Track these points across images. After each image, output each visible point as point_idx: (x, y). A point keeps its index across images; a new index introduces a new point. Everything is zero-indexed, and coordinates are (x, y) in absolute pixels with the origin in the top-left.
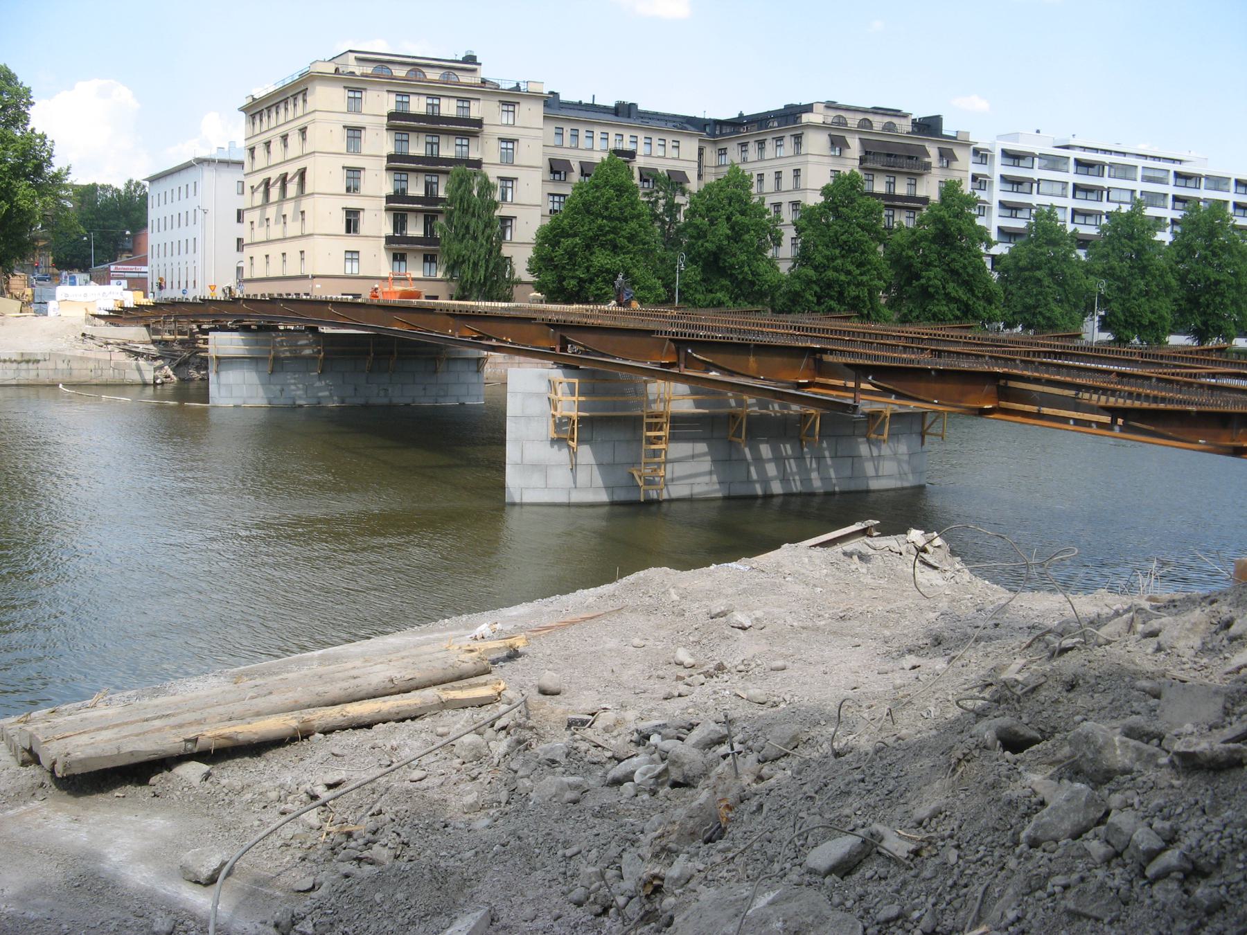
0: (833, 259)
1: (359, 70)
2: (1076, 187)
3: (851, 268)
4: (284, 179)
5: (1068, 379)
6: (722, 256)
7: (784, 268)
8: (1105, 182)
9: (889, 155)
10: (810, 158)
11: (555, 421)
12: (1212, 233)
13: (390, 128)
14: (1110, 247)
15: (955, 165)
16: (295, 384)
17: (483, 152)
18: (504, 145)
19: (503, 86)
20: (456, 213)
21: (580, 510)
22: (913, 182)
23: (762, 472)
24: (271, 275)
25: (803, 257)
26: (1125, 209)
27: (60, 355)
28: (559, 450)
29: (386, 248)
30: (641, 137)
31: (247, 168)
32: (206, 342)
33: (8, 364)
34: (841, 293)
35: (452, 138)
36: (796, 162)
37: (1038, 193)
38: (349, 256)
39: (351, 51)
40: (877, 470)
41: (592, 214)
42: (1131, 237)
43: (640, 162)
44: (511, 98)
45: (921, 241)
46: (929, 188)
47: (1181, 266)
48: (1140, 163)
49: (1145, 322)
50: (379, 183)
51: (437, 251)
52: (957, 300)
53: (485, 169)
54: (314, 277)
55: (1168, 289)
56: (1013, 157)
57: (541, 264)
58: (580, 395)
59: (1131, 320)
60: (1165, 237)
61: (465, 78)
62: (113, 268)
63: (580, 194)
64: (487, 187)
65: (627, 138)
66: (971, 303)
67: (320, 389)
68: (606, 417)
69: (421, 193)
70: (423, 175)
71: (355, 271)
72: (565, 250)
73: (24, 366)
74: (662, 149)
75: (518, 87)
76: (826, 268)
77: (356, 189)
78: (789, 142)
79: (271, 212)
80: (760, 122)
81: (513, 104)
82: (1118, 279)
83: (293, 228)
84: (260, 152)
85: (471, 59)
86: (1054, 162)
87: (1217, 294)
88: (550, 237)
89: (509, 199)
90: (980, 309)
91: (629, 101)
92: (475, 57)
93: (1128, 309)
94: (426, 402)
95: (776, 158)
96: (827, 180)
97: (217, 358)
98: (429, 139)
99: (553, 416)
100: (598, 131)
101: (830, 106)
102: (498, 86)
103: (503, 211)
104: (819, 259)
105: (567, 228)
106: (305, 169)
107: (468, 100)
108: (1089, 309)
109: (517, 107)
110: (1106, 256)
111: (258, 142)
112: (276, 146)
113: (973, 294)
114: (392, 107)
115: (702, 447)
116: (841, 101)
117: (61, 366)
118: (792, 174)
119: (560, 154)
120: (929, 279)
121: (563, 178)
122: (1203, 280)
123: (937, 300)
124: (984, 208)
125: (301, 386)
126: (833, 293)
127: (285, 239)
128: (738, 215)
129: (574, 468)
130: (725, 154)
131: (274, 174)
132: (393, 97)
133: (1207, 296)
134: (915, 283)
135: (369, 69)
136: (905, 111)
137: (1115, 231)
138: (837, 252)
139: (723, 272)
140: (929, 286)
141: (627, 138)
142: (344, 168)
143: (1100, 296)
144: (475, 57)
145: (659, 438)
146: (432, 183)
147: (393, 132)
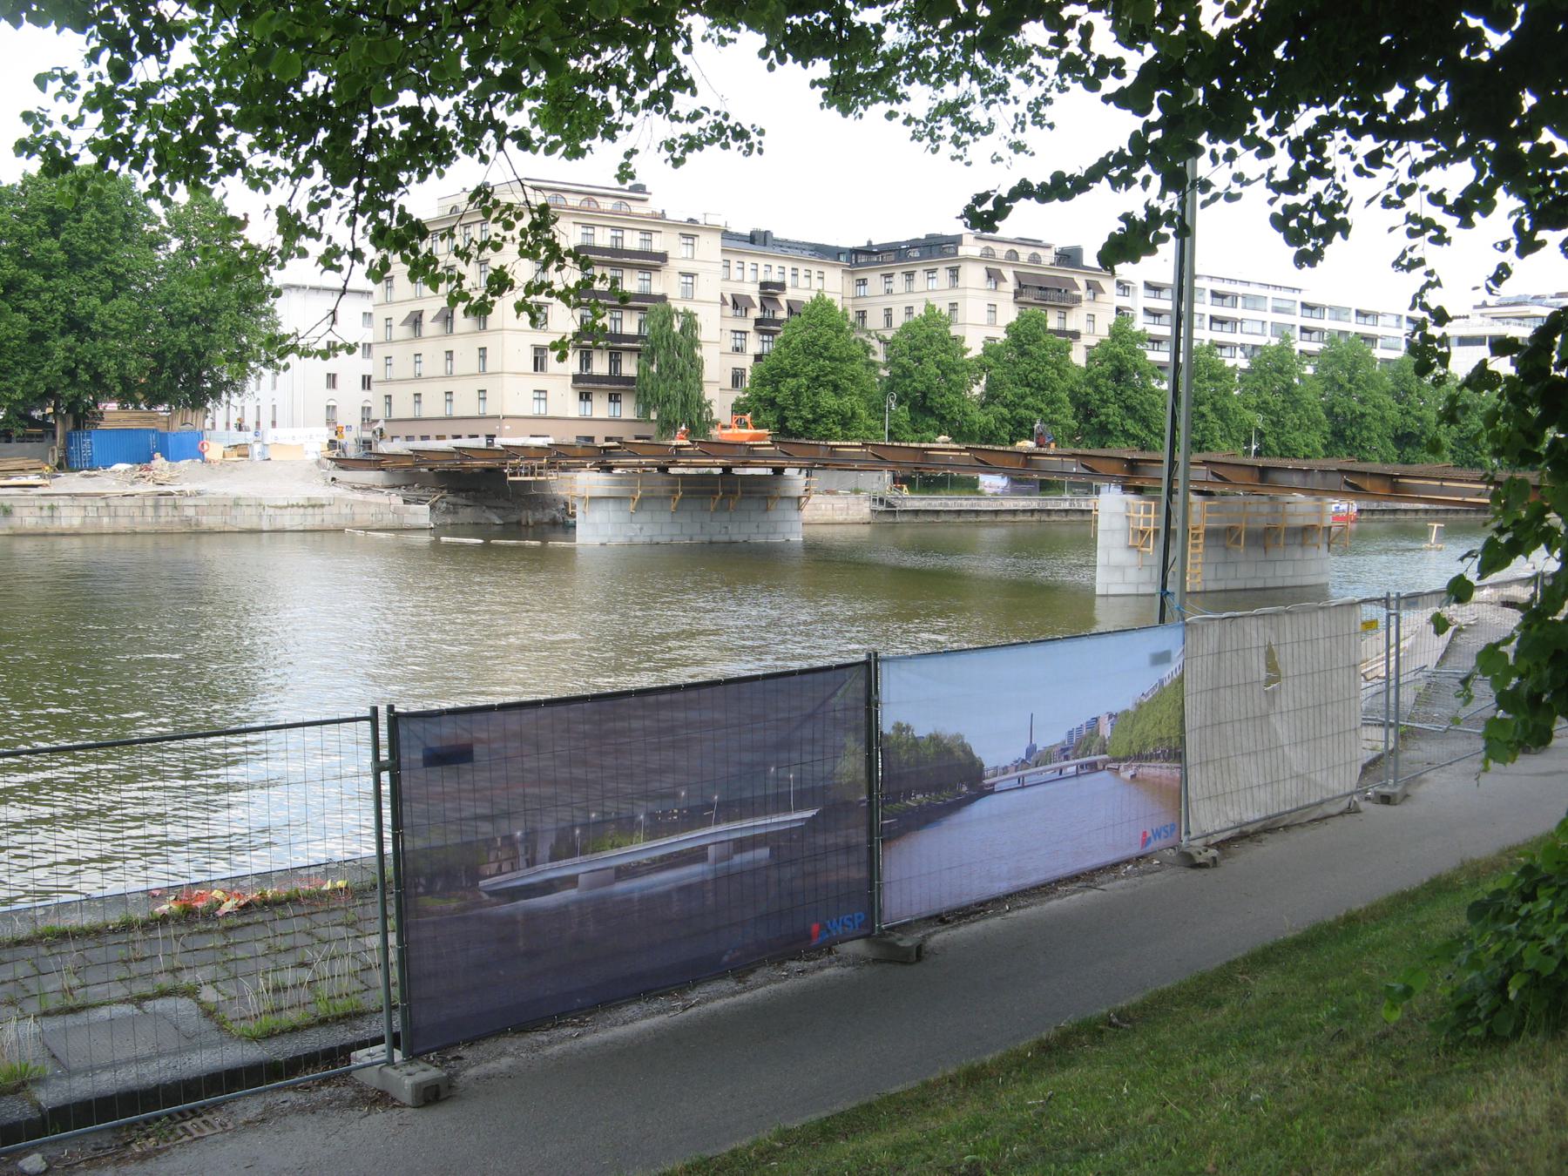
0: (1023, 397)
3: (1043, 406)
8: (1236, 313)
9: (1040, 288)
10: (969, 292)
15: (1100, 297)
18: (684, 279)
26: (1275, 341)
27: (343, 500)
30: (789, 266)
33: (295, 509)
36: (953, 296)
38: (537, 395)
42: (1280, 371)
44: (690, 230)
48: (1271, 293)
55: (1317, 423)
65: (775, 269)
71: (543, 412)
73: (310, 510)
74: (740, 272)
78: (943, 275)
81: (692, 237)
82: (1272, 413)
91: (764, 229)
93: (1284, 444)
94: (761, 540)
95: (928, 291)
100: (748, 261)
107: (650, 232)
113: (1150, 431)
117: (346, 511)
120: (1107, 415)
130: (864, 284)
132: (579, 229)
136: (1046, 241)
139: (930, 411)
141: (775, 269)
143: (1257, 430)
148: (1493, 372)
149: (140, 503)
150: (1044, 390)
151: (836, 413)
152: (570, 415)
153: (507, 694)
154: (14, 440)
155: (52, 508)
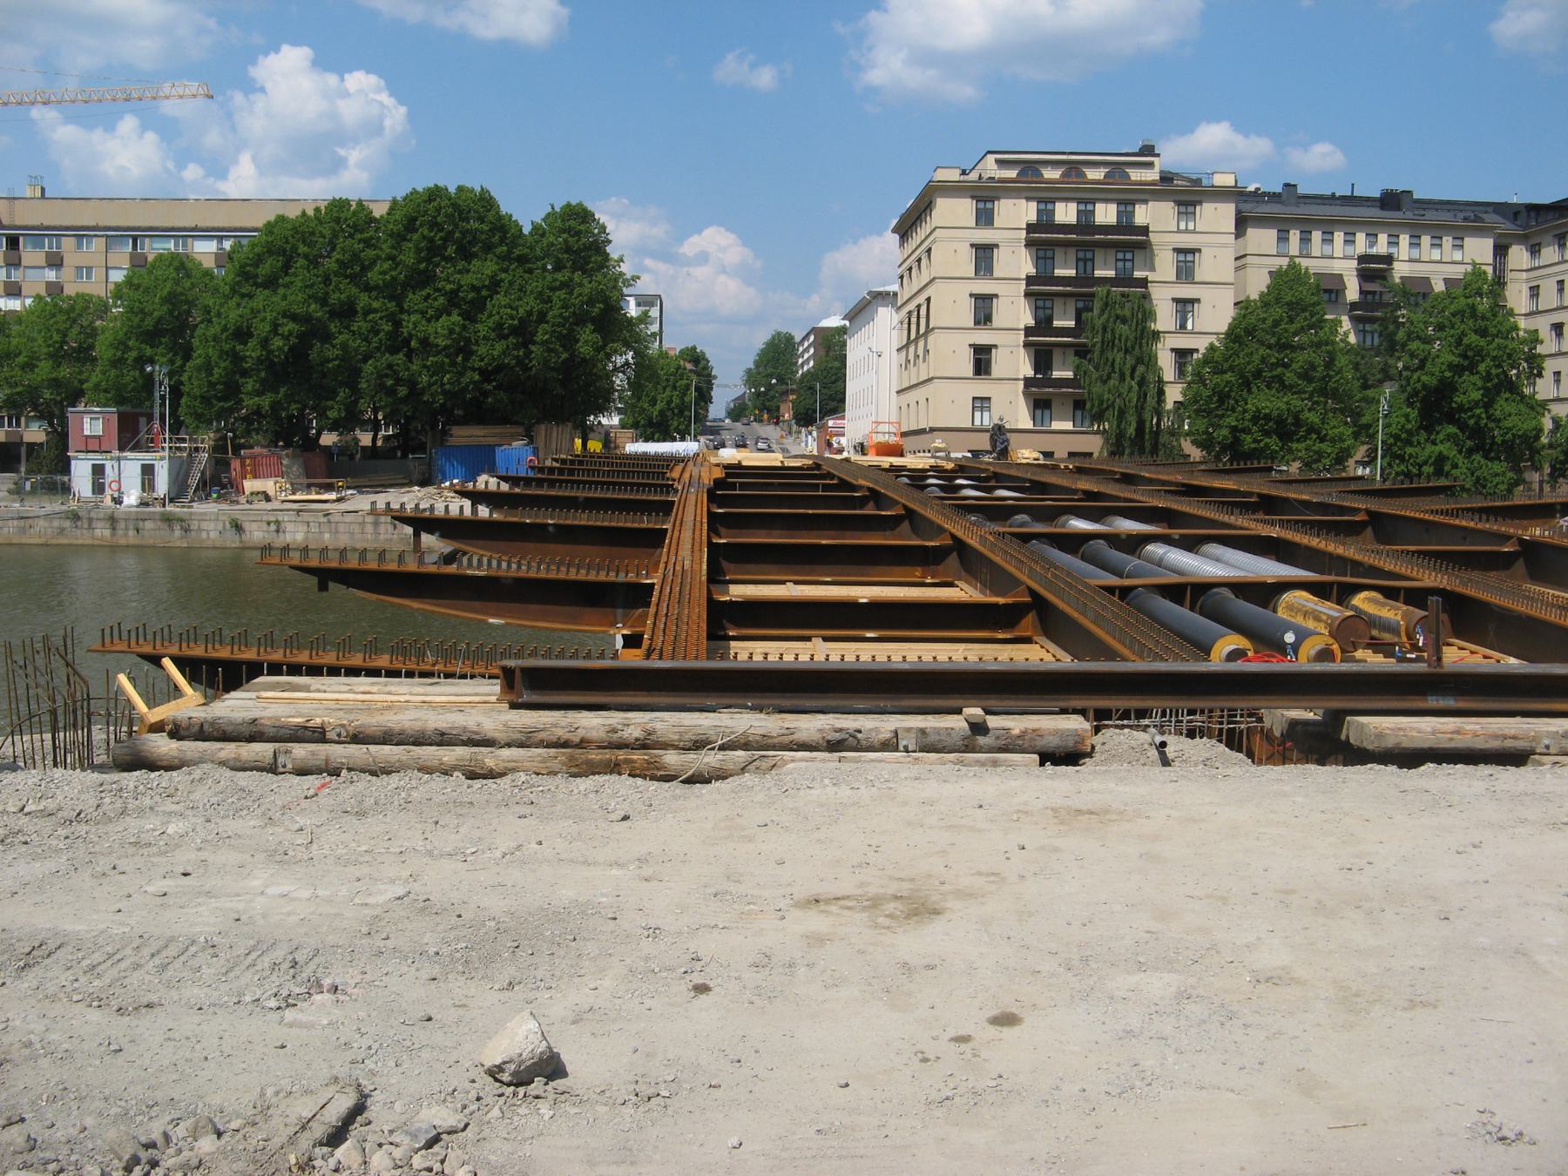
17: (1153, 269)
18: (1182, 257)
29: (1024, 393)
50: (1016, 313)
61: (1136, 175)
62: (831, 423)
70: (1073, 299)
85: (1148, 150)
89: (1189, 327)
95: (1179, 231)
98: (1081, 255)
109: (1198, 208)
132: (1033, 205)
135: (1012, 174)
142: (971, 295)
147: (1034, 249)
148: (300, 45)
149: (360, 520)
151: (1267, 417)
152: (1021, 426)
154: (1393, 250)
155: (277, 522)
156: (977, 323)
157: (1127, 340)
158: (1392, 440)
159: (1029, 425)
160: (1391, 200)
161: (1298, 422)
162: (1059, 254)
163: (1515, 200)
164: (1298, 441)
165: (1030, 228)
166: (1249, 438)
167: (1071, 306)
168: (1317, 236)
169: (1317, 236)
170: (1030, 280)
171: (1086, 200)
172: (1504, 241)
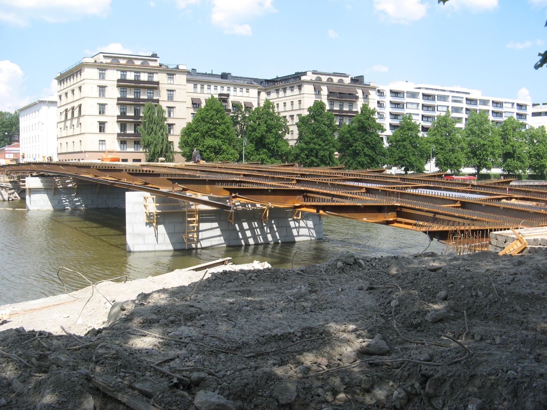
0: (313, 139)
1: (105, 61)
2: (423, 106)
3: (321, 143)
4: (73, 109)
5: (329, 192)
6: (263, 139)
7: (292, 143)
11: (147, 215)
12: (481, 124)
13: (118, 86)
14: (437, 131)
16: (65, 200)
17: (160, 96)
18: (169, 93)
19: (170, 67)
20: (147, 123)
21: (140, 254)
22: (351, 105)
23: (244, 235)
24: (75, 151)
25: (300, 138)
28: (150, 227)
29: (117, 139)
31: (59, 105)
32: (24, 182)
34: (317, 154)
35: (146, 90)
37: (407, 108)
39: (101, 53)
40: (298, 233)
41: (205, 122)
42: (445, 126)
43: (231, 99)
44: (171, 73)
45: (352, 130)
46: (358, 107)
47: (469, 139)
48: (451, 94)
49: (452, 162)
50: (113, 110)
51: (140, 139)
52: (369, 156)
53: (161, 103)
54: (85, 152)
56: (395, 93)
57: (183, 144)
58: (156, 203)
59: (446, 162)
60: (461, 125)
61: (152, 64)
63: (200, 114)
64: (161, 111)
66: (374, 157)
67: (77, 202)
68: (169, 212)
69: (133, 114)
72: (193, 138)
75: (177, 68)
76: (310, 143)
77: (103, 113)
79: (68, 123)
80: (285, 79)
82: (441, 144)
83: (77, 131)
84: (63, 97)
85: (154, 55)
86: (413, 95)
87: (484, 150)
88: (188, 131)
90: (379, 159)
92: (156, 54)
95: (168, 84)
96: (311, 104)
97: (30, 189)
98: (136, 91)
99: (146, 213)
101: (314, 73)
102: (168, 67)
103: (170, 121)
104: (307, 139)
105: (194, 128)
106: (81, 105)
108: (428, 159)
109: (174, 76)
110: (435, 135)
111: (63, 93)
112: (70, 94)
114: (119, 77)
115: (216, 225)
116: (319, 71)
118: (283, 104)
119: (196, 96)
120: (356, 147)
121: (382, 95)
122: (477, 144)
123: (360, 155)
124: (382, 117)
125: (67, 200)
126: (313, 154)
127: (81, 134)
128: (269, 121)
129: (156, 236)
131: (69, 107)
132: (119, 73)
133: (480, 151)
134: (350, 148)
135: (109, 61)
136: (347, 74)
137: (439, 124)
138: (315, 135)
139: (264, 146)
140: (356, 150)
142: (98, 104)
144: (156, 54)
145: (194, 221)
146: (137, 110)
147: (120, 88)
150: (322, 135)
151: (211, 147)
153: (366, 201)
156: (100, 113)
157: (157, 121)
158: (247, 154)
159: (119, 149)
160: (224, 76)
161: (220, 149)
162: (128, 90)
163: (261, 78)
164: (220, 155)
165: (119, 81)
166: (205, 154)
167: (133, 108)
168: (206, 87)
169: (206, 87)
170: (119, 99)
171: (137, 72)
172: (260, 91)
